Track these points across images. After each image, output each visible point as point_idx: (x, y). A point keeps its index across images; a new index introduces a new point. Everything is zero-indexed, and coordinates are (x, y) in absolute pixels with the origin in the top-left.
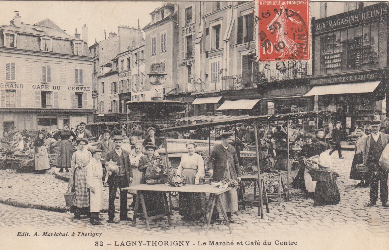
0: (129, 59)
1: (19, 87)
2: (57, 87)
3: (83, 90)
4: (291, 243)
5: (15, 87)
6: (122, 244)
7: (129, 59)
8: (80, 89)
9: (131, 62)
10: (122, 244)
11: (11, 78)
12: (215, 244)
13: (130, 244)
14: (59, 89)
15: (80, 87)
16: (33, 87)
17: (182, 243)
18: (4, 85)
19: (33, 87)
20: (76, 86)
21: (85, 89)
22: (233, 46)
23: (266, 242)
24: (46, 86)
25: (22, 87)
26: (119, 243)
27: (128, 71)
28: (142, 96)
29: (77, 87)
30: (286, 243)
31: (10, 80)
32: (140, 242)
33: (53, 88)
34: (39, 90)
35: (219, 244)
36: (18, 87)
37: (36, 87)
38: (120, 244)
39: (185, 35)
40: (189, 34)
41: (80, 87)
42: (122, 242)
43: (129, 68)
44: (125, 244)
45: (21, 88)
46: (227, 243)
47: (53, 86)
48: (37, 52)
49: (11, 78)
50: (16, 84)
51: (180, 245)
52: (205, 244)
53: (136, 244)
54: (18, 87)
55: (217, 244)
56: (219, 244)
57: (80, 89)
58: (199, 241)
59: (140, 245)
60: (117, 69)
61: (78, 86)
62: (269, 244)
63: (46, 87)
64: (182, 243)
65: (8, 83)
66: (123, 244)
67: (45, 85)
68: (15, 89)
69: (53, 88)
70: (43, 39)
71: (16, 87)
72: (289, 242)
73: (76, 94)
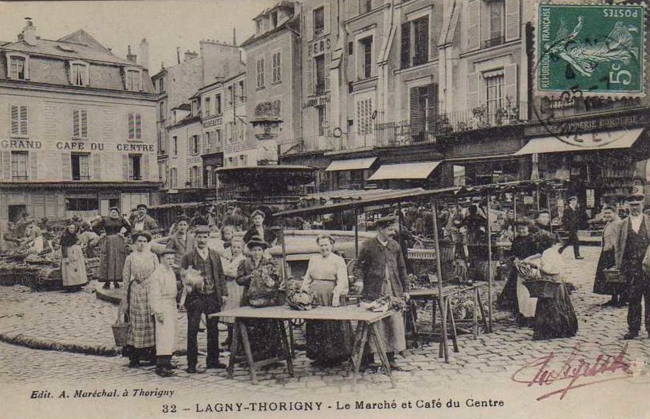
0: (218, 97)
1: (34, 146)
2: (98, 146)
3: (141, 149)
4: (493, 403)
5: (28, 147)
6: (209, 408)
7: (218, 97)
8: (137, 149)
9: (222, 101)
10: (209, 408)
11: (19, 130)
12: (364, 406)
13: (222, 408)
14: (101, 148)
15: (136, 144)
16: (118, 147)
17: (309, 406)
18: (9, 143)
19: (118, 147)
20: (129, 144)
21: (145, 147)
22: (394, 72)
23: (451, 403)
24: (79, 144)
25: (38, 146)
26: (203, 406)
27: (216, 117)
28: (242, 159)
29: (132, 145)
30: (484, 404)
31: (19, 135)
32: (319, 404)
33: (92, 147)
34: (68, 151)
35: (372, 406)
36: (32, 146)
37: (64, 146)
38: (205, 410)
39: (314, 55)
40: (319, 53)
41: (136, 144)
42: (209, 405)
43: (219, 111)
44: (213, 408)
45: (36, 147)
46: (385, 404)
47: (92, 145)
48: (64, 87)
49: (19, 133)
50: (28, 142)
51: (306, 410)
52: (347, 407)
53: (231, 409)
54: (32, 146)
55: (369, 406)
56: (372, 406)
57: (137, 149)
58: (197, 405)
59: (239, 410)
60: (200, 112)
61: (133, 144)
62: (456, 405)
63: (79, 146)
64: (309, 406)
65: (16, 140)
66: (210, 409)
67: (77, 142)
68: (27, 149)
69: (92, 147)
70: (74, 64)
71: (30, 146)
72: (490, 401)
73: (130, 156)
